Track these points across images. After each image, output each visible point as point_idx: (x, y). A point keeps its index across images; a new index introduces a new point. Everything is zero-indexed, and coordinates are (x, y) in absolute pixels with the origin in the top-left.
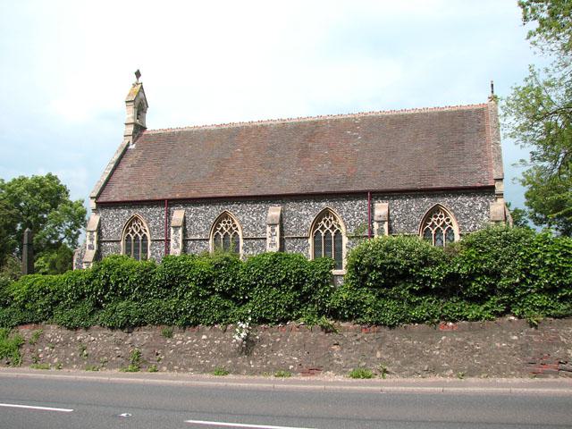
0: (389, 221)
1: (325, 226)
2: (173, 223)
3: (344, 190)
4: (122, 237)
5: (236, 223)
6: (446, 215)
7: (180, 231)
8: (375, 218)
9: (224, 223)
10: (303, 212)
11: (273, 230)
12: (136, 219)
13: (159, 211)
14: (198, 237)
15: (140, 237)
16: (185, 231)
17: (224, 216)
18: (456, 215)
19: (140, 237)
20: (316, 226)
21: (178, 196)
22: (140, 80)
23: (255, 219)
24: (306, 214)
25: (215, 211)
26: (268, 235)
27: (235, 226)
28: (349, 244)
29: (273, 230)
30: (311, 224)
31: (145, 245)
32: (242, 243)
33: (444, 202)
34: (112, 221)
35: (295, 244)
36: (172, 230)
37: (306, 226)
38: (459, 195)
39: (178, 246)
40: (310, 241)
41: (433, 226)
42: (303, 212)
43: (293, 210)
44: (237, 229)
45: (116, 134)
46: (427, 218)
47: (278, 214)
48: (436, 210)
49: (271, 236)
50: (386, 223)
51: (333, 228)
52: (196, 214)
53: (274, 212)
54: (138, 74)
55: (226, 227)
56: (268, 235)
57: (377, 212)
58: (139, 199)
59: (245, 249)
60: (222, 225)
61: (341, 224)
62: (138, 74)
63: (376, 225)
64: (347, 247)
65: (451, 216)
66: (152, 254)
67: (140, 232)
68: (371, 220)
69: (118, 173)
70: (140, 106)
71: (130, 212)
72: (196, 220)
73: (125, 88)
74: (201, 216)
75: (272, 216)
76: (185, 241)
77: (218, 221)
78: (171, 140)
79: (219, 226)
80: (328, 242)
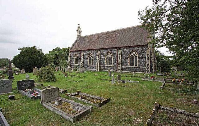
2: (81, 55)
6: (135, 53)
7: (82, 57)
12: (109, 53)
13: (79, 52)
18: (138, 53)
24: (105, 53)
25: (88, 52)
27: (136, 54)
33: (134, 49)
40: (129, 59)
41: (132, 55)
45: (74, 39)
46: (131, 53)
48: (133, 51)
51: (135, 55)
53: (99, 53)
54: (79, 25)
57: (119, 52)
61: (137, 54)
62: (79, 25)
65: (136, 53)
67: (110, 56)
68: (117, 54)
69: (75, 45)
70: (80, 32)
78: (85, 37)
80: (109, 59)
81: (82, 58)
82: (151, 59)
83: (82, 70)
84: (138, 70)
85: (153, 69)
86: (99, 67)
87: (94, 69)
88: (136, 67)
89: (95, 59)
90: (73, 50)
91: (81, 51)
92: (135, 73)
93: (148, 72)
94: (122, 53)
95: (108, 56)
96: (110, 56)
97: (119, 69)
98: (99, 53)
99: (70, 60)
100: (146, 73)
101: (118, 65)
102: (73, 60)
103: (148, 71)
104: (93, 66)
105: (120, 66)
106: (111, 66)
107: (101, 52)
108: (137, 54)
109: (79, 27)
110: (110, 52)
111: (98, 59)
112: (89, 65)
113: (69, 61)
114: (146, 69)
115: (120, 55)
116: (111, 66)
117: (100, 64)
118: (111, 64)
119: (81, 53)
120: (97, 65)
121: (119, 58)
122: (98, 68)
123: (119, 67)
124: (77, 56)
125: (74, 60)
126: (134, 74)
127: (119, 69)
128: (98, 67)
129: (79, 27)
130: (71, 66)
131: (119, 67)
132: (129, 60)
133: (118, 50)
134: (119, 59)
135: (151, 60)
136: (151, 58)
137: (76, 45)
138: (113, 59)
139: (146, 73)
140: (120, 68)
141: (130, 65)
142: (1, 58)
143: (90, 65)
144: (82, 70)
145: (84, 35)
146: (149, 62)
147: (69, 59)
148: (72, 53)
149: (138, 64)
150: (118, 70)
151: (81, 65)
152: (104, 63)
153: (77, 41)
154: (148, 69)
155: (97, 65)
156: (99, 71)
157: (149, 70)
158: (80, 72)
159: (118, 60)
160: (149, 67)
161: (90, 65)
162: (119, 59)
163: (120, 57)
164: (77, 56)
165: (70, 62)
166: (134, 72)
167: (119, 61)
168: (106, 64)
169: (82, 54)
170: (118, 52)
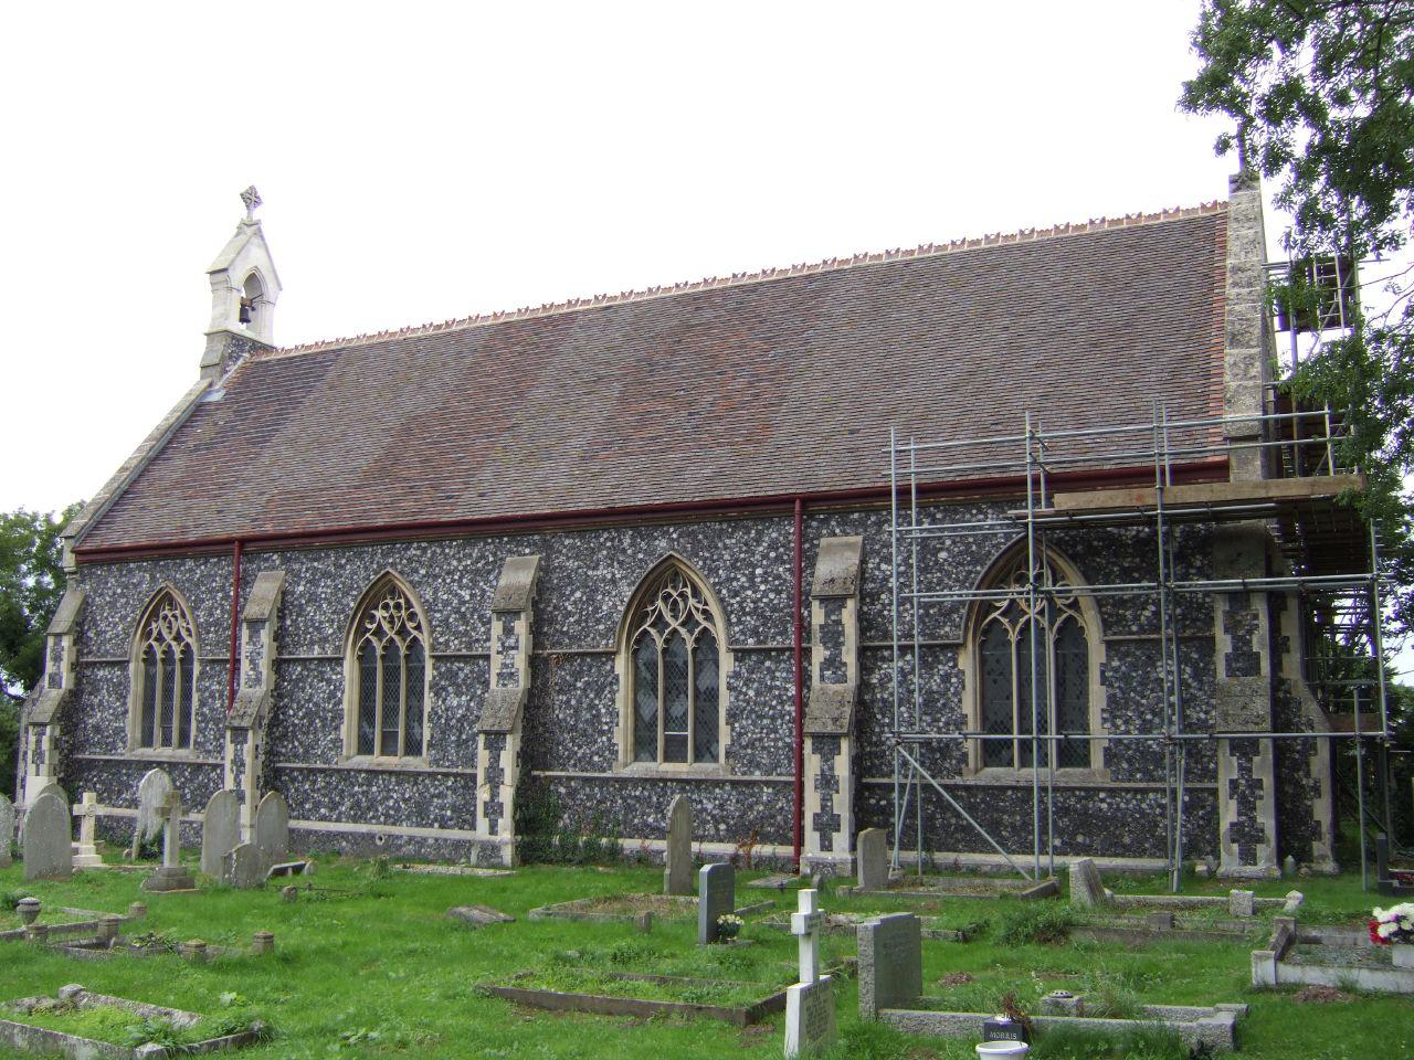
0: (866, 597)
1: (668, 617)
2: (251, 610)
3: (723, 493)
4: (137, 648)
5: (417, 609)
7: (265, 636)
8: (816, 589)
9: (386, 607)
10: (602, 571)
11: (508, 631)
13: (220, 571)
14: (316, 652)
15: (177, 649)
16: (279, 636)
17: (383, 590)
19: (177, 649)
20: (640, 617)
21: (269, 528)
22: (257, 214)
23: (466, 595)
25: (359, 571)
26: (495, 645)
27: (412, 616)
28: (736, 675)
29: (508, 631)
30: (621, 608)
31: (416, 675)
32: (429, 674)
34: (112, 605)
35: (577, 675)
36: (245, 633)
37: (609, 616)
38: (184, 557)
39: (258, 681)
40: (621, 665)
42: (602, 571)
43: (570, 564)
44: (418, 628)
47: (853, 560)
49: (505, 649)
50: (851, 604)
52: (313, 582)
53: (518, 574)
54: (251, 198)
55: (391, 621)
56: (495, 645)
58: (175, 540)
59: (438, 690)
60: (380, 614)
61: (714, 608)
62: (251, 198)
63: (818, 616)
64: (730, 688)
66: (203, 704)
67: (689, 622)
68: (802, 598)
69: (161, 470)
71: (153, 578)
72: (313, 599)
73: (213, 239)
74: (324, 589)
75: (508, 587)
76: (279, 665)
77: (369, 602)
78: (314, 365)
79: (373, 618)
81: (257, 652)
82: (1276, 666)
83: (247, 837)
84: (1116, 820)
85: (1322, 810)
86: (520, 792)
87: (434, 832)
88: (1074, 776)
89: (466, 665)
90: (122, 535)
91: (245, 549)
92: (1096, 880)
93: (1248, 856)
94: (865, 588)
95: (660, 622)
96: (689, 622)
97: (827, 825)
98: (518, 574)
99: (67, 681)
100: (1230, 862)
101: (813, 764)
102: (120, 690)
103: (1247, 837)
104: (416, 776)
105: (842, 766)
106: (705, 769)
107: (544, 571)
108: (714, 608)
109: (251, 230)
110: (694, 570)
111: (507, 676)
112: (365, 761)
113: (50, 698)
114: (1229, 814)
115: (834, 602)
116: (705, 769)
117: (527, 741)
118: (704, 750)
119: (243, 582)
120: (483, 757)
121: (819, 654)
122: (493, 809)
123: (827, 782)
124: (185, 626)
125: (136, 687)
126: (1079, 892)
127: (827, 825)
128: (507, 795)
129: (251, 230)
130: (71, 777)
131: (827, 782)
132: (970, 680)
133: (802, 537)
134: (833, 663)
135: (1277, 683)
136: (1278, 646)
137: (179, 463)
138: (727, 663)
139: (1230, 862)
140: (842, 804)
141: (365, 746)
142: (9, 508)
143: (376, 760)
144: (247, 837)
145: (289, 345)
146: (1261, 705)
147: (59, 666)
148: (112, 580)
149: (724, 738)
150: (812, 838)
151: (239, 762)
152: (596, 727)
153: (196, 411)
154: (1247, 806)
155: (483, 757)
156: (507, 854)
157: (1266, 820)
158: (204, 867)
159: (803, 680)
160: (1268, 781)
161: (376, 760)
162: (833, 663)
163: (833, 636)
164: (185, 626)
165: (71, 713)
166: (1074, 863)
167: (831, 696)
168: (622, 737)
169: (265, 589)
170: (805, 559)
